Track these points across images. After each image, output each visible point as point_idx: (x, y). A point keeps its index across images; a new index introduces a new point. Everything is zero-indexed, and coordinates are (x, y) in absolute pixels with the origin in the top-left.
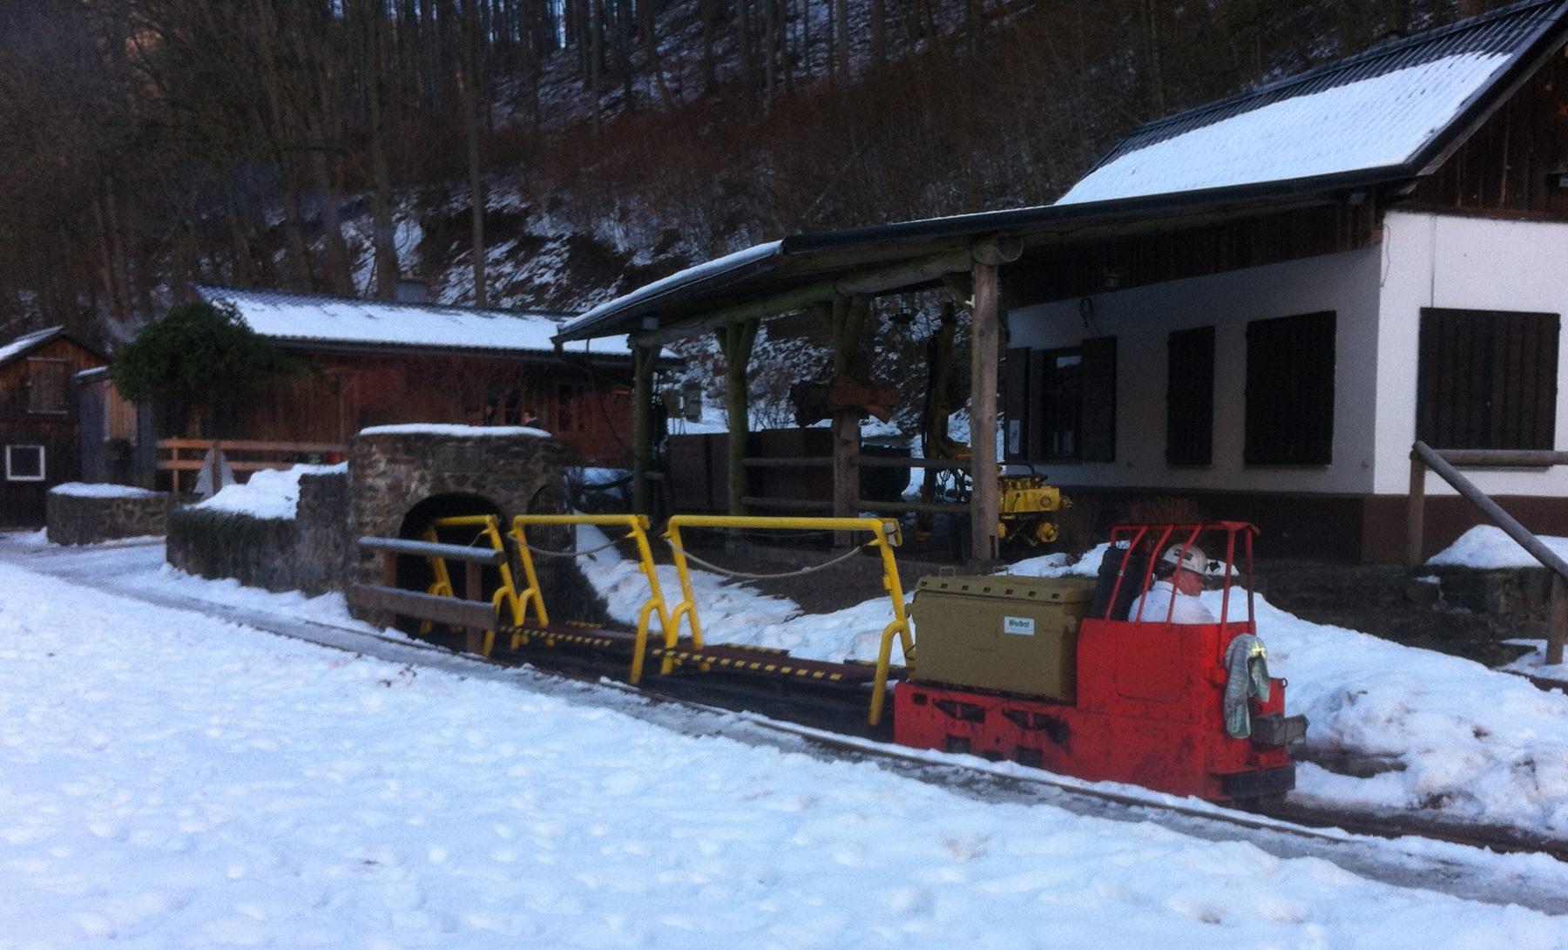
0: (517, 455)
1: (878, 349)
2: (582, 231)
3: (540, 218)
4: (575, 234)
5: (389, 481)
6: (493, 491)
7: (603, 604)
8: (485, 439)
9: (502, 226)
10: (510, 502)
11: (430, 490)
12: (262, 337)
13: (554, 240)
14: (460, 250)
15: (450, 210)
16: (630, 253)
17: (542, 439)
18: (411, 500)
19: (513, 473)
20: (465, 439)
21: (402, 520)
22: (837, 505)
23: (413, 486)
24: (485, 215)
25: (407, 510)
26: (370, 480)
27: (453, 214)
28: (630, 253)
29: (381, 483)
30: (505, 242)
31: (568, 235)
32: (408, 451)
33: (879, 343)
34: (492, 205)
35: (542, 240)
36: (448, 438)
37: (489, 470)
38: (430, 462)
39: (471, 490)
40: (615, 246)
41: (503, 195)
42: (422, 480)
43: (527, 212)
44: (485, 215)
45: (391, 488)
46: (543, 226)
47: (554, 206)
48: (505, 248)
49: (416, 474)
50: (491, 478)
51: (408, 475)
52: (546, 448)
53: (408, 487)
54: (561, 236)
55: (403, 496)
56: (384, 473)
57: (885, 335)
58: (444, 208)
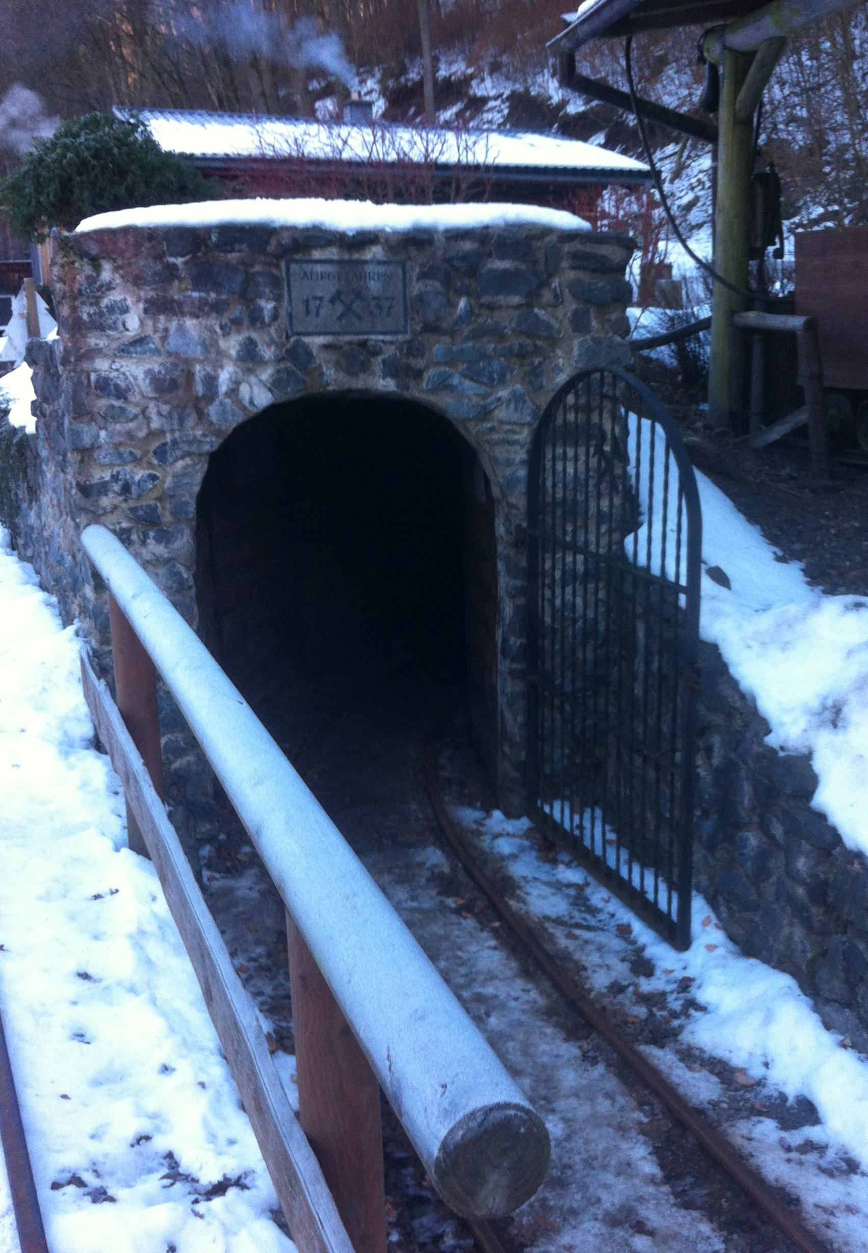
0: (504, 281)
1: (827, 169)
2: (519, 87)
3: (483, 80)
4: (513, 92)
5: (155, 365)
6: (443, 385)
7: (793, 778)
8: (416, 240)
9: (450, 91)
10: (485, 413)
11: (275, 385)
12: (169, 155)
13: (496, 98)
14: (416, 115)
15: (407, 80)
16: (564, 103)
17: (570, 236)
18: (223, 416)
19: (497, 333)
20: (365, 238)
21: (202, 468)
22: (320, 274)
23: (225, 376)
24: (435, 82)
25: (211, 444)
26: (102, 365)
27: (409, 84)
28: (564, 103)
29: (135, 371)
30: (453, 104)
31: (507, 93)
32: (204, 276)
33: (828, 163)
34: (443, 73)
35: (484, 100)
36: (315, 237)
37: (431, 328)
38: (268, 306)
39: (386, 385)
40: (550, 98)
41: (450, 64)
42: (249, 356)
43: (472, 77)
44: (435, 82)
45: (164, 386)
46: (485, 87)
47: (495, 68)
48: (455, 109)
49: (232, 345)
50: (438, 347)
51: (209, 345)
52: (581, 261)
53: (211, 381)
54: (501, 95)
55: (199, 406)
56: (140, 341)
57: (832, 155)
58: (403, 80)
